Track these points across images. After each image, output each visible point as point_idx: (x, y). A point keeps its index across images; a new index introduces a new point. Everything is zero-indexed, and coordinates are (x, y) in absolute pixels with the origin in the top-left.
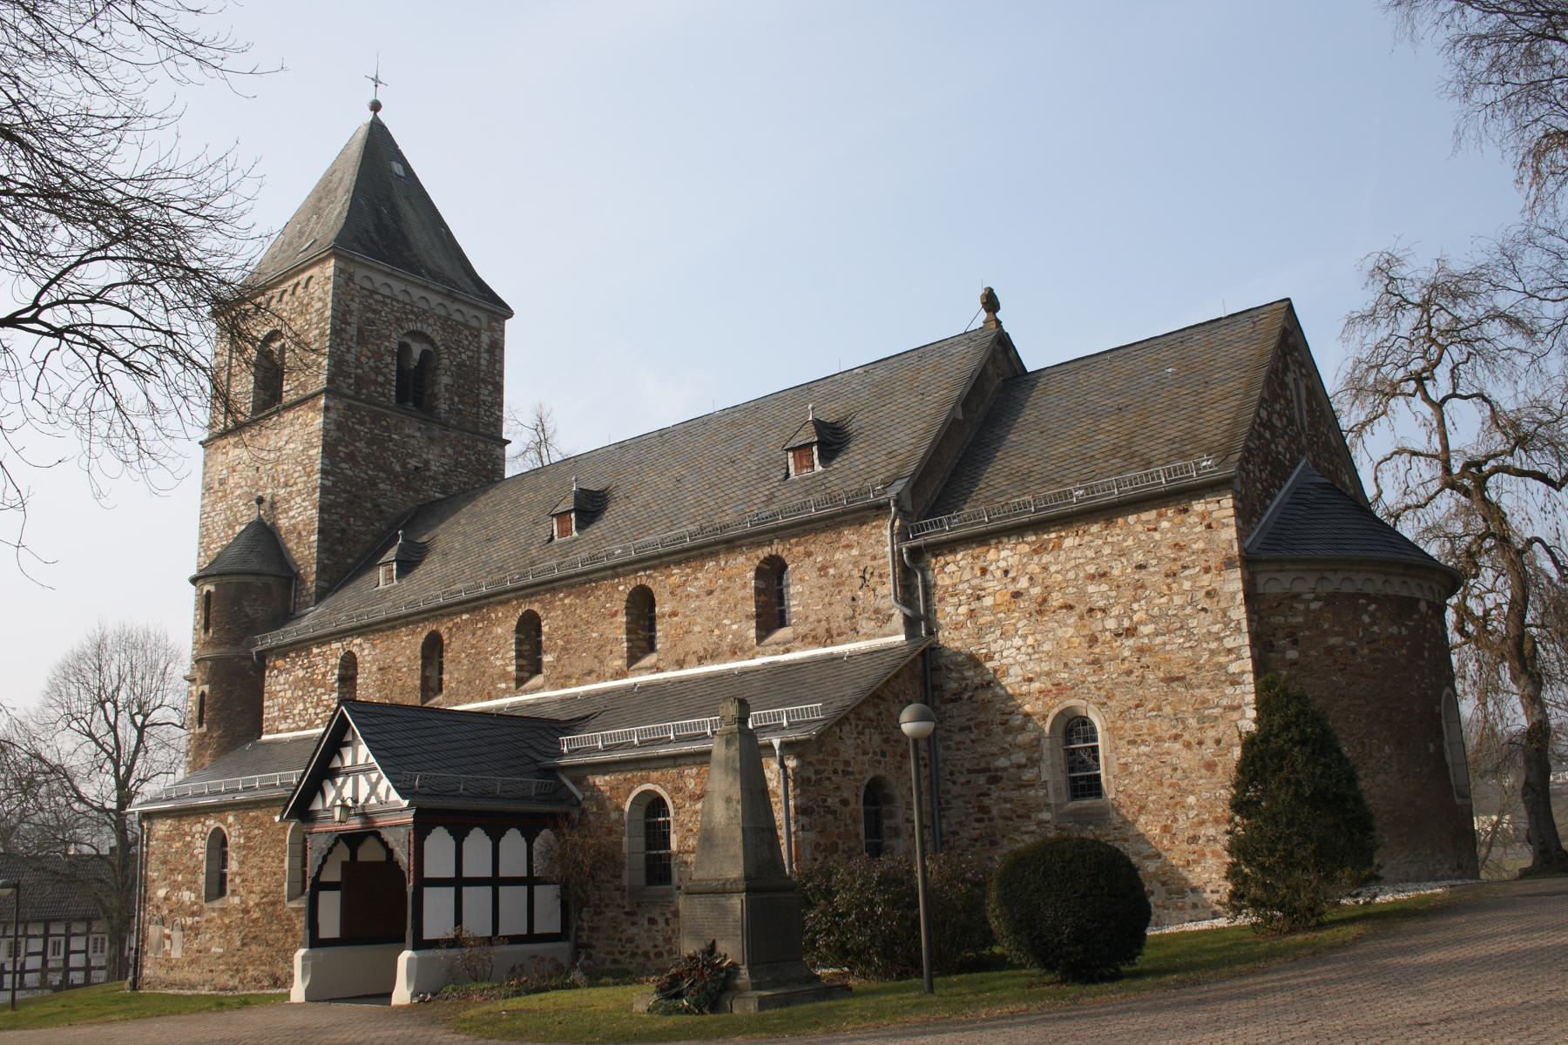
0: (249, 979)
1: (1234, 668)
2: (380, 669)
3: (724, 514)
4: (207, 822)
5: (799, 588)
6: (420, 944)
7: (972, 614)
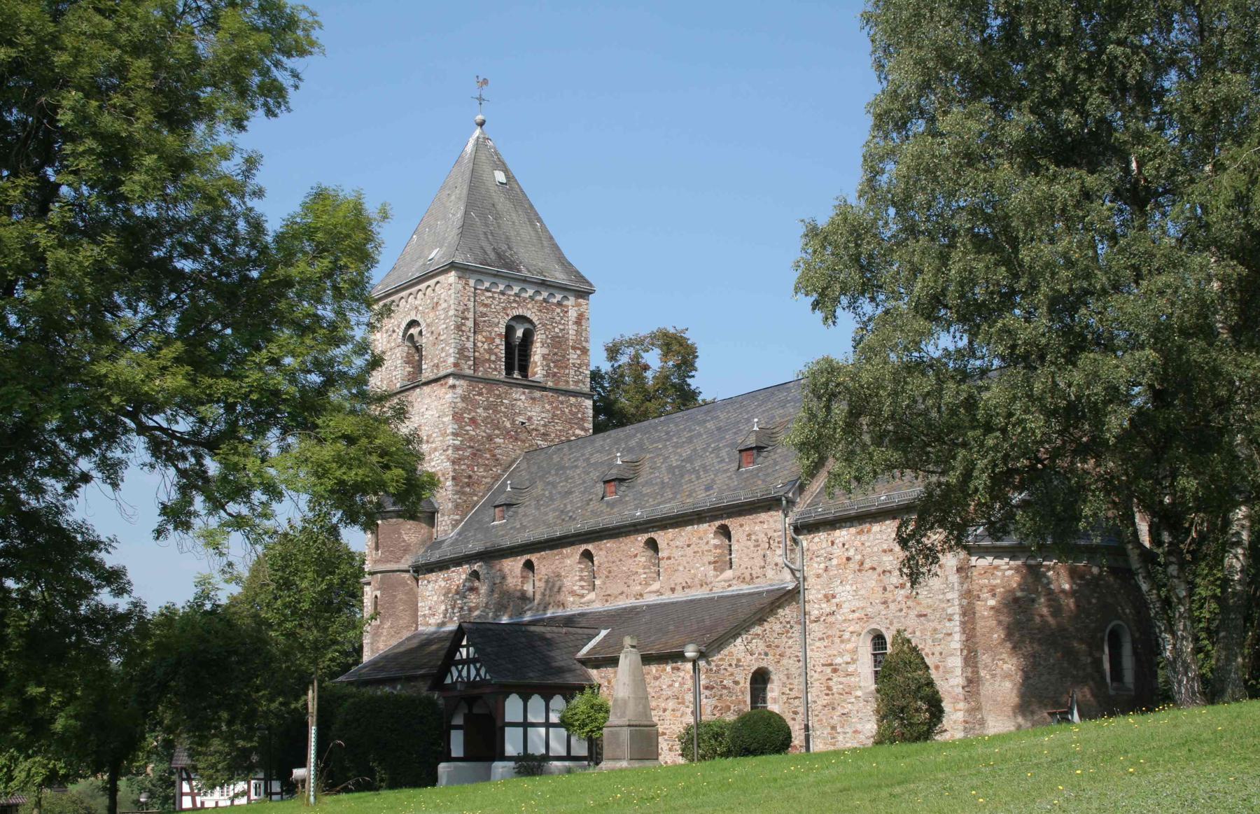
1: (950, 611)
7: (826, 569)
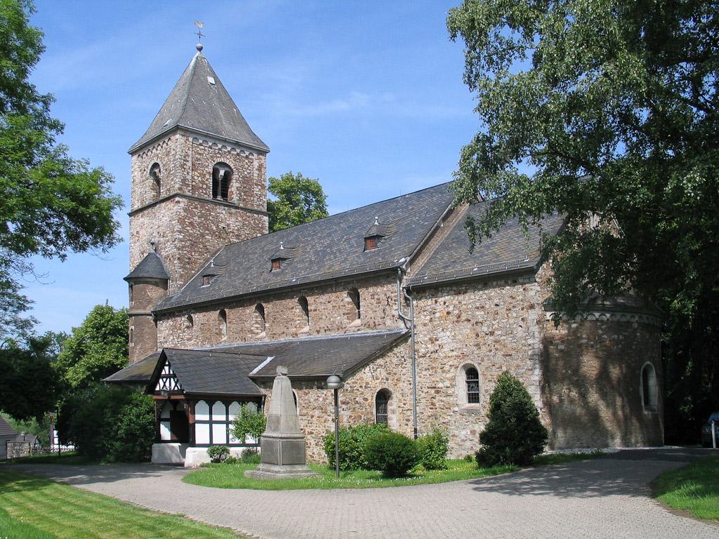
7: (431, 320)
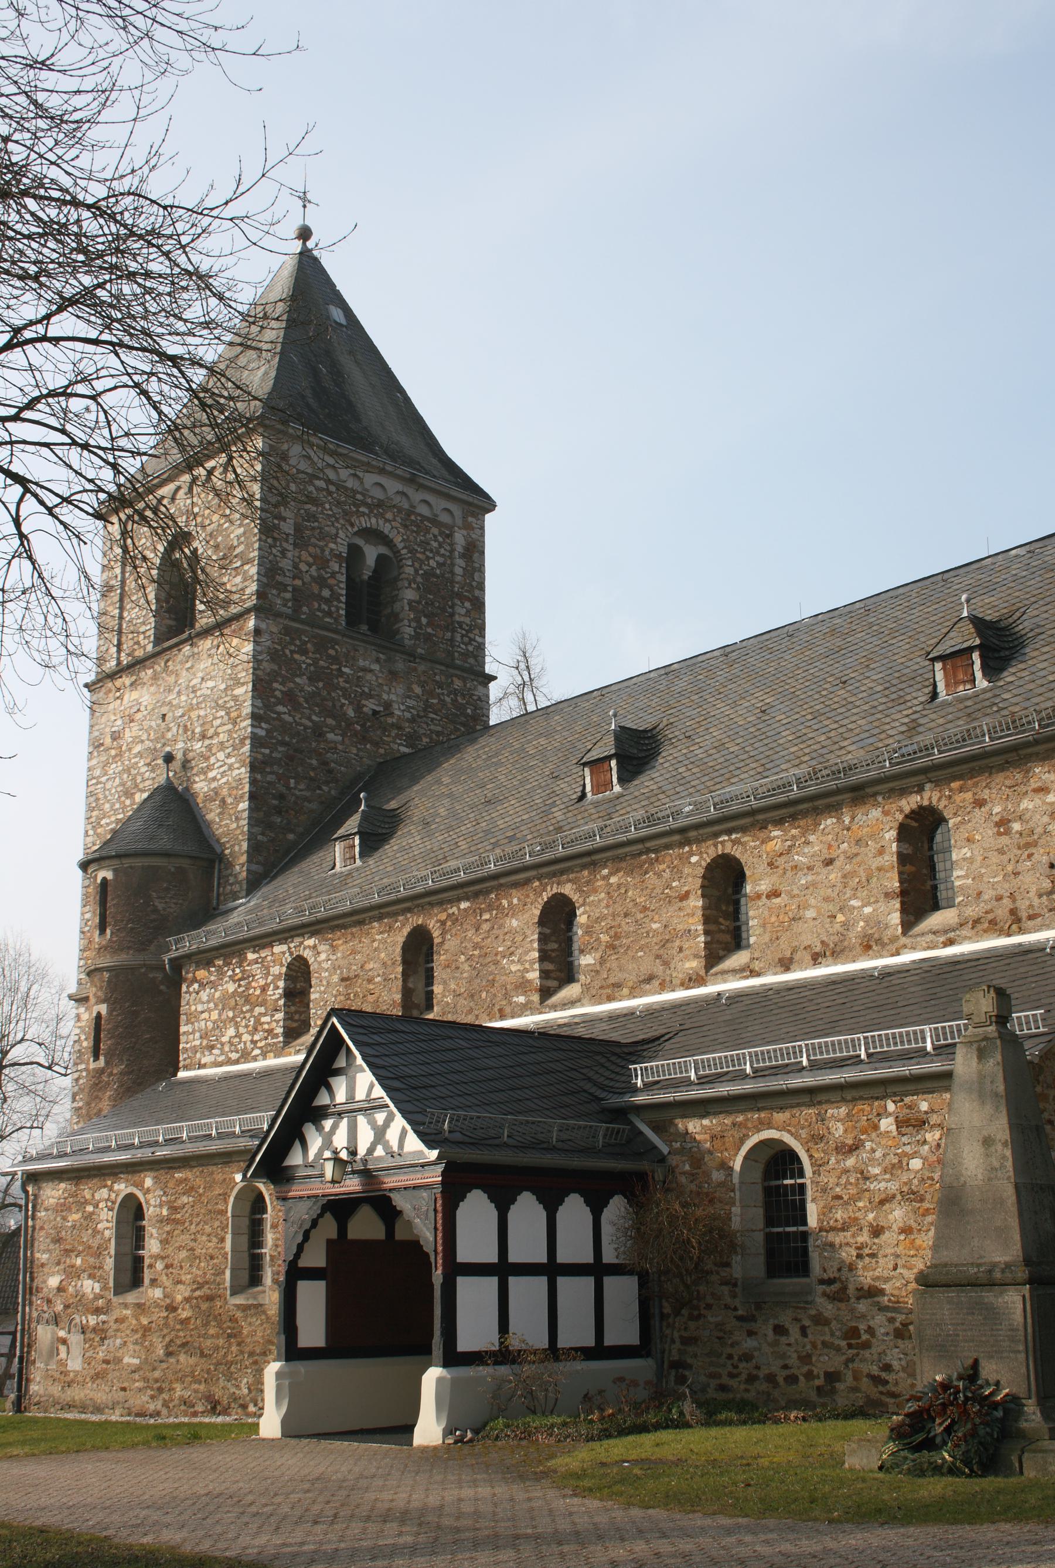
0: (176, 1402)
2: (343, 980)
3: (843, 752)
4: (116, 1187)
5: (966, 852)
6: (453, 1358)
